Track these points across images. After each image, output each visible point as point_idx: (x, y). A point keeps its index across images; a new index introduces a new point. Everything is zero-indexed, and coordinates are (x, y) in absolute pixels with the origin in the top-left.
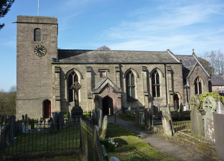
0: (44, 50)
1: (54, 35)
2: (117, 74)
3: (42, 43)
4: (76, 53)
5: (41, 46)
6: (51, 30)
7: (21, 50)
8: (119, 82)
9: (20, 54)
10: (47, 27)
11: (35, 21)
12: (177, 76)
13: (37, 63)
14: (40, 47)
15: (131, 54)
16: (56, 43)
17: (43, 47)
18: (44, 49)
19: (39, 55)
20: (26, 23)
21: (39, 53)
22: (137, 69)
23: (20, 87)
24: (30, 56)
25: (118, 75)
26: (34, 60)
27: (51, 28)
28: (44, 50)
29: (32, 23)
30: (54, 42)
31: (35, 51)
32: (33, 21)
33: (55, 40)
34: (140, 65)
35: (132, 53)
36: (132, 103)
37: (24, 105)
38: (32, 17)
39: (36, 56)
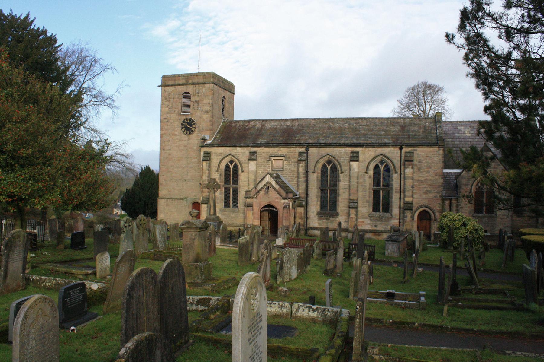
2: (300, 165)
7: (166, 127)
8: (303, 179)
9: (164, 132)
12: (428, 172)
13: (185, 146)
19: (187, 133)
20: (172, 85)
22: (341, 157)
24: (176, 135)
25: (302, 166)
29: (179, 85)
32: (181, 82)
34: (347, 148)
36: (327, 219)
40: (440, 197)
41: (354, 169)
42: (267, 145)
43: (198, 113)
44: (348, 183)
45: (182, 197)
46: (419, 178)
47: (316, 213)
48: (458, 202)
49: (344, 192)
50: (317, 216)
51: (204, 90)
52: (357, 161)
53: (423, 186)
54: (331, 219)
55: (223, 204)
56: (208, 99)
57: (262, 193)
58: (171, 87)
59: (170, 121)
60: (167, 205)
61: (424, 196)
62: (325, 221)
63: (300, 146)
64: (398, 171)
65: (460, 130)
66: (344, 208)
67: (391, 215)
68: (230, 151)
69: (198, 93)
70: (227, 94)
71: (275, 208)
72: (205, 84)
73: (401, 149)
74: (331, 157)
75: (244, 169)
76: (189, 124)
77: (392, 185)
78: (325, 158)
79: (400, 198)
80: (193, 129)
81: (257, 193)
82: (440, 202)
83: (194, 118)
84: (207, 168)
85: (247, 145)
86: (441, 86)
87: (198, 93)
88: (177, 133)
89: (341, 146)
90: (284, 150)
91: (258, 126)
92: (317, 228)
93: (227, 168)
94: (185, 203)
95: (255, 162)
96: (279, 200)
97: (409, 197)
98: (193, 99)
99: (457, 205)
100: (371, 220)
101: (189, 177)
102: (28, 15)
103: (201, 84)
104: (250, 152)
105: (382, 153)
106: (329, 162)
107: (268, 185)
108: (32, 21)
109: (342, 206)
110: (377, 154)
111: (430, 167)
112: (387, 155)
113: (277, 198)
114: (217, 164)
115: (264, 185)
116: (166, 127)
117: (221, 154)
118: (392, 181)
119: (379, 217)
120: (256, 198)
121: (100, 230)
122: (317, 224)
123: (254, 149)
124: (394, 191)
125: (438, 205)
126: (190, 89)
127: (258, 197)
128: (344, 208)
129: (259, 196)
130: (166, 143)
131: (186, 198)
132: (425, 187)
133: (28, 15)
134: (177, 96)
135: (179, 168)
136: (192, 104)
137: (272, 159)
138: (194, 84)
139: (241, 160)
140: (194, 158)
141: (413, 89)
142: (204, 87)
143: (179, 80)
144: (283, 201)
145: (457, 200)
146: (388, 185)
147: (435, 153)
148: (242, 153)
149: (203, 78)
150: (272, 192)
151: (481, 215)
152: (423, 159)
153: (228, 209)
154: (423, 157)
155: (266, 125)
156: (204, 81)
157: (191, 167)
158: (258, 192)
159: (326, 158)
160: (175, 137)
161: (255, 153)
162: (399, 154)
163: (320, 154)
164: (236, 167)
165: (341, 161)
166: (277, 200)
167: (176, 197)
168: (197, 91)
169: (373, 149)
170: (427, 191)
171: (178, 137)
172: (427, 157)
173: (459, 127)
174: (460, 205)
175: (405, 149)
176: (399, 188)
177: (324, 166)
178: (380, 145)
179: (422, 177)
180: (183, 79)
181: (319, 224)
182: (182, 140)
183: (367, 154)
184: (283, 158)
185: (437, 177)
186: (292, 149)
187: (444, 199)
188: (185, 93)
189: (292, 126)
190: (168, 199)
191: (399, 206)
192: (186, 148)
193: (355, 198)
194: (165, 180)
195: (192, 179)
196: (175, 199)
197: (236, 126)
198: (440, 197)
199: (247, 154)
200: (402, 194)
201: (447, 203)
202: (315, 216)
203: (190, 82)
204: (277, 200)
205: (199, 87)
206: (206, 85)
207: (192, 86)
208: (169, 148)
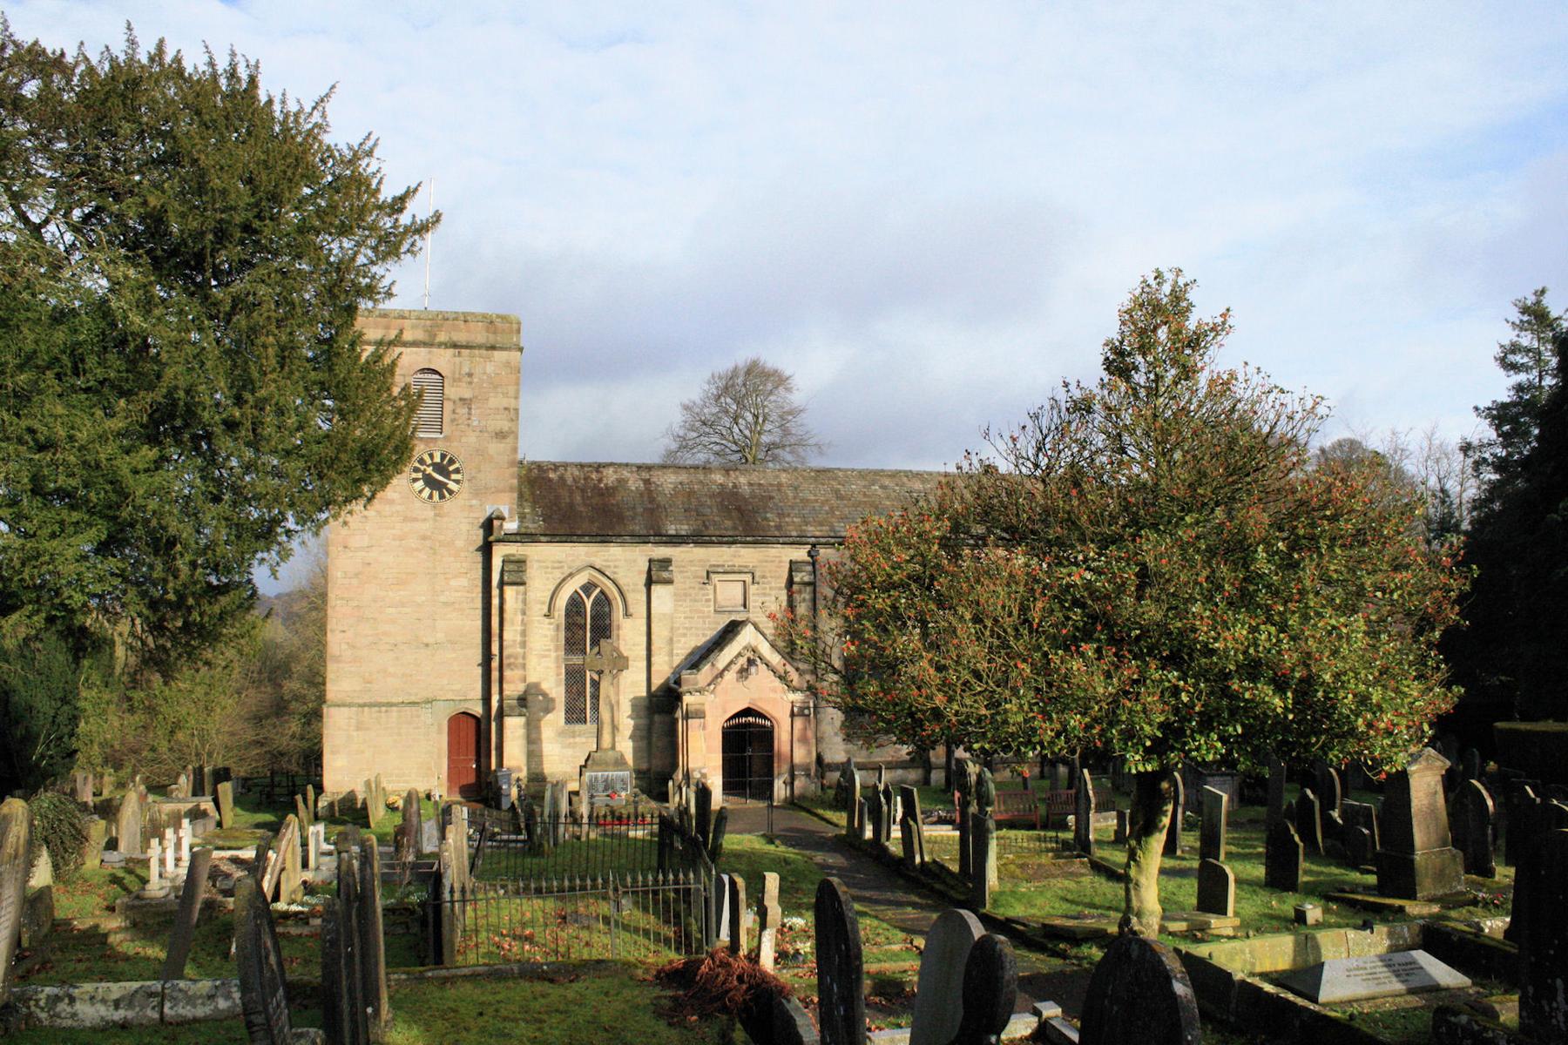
0: (454, 476)
1: (505, 402)
3: (446, 439)
4: (600, 480)
5: (443, 456)
6: (489, 376)
10: (466, 360)
11: (420, 335)
13: (424, 538)
14: (437, 459)
15: (880, 492)
16: (510, 440)
17: (452, 462)
18: (457, 471)
19: (431, 497)
21: (432, 488)
23: (344, 647)
26: (406, 519)
27: (490, 368)
28: (420, 475)
30: (501, 435)
31: (415, 480)
33: (505, 425)
35: (887, 482)
37: (358, 728)
38: (466, 318)
39: (418, 504)
42: (698, 538)
43: (472, 439)
45: (413, 699)
56: (506, 395)
57: (730, 676)
60: (359, 727)
63: (796, 543)
68: (587, 554)
72: (493, 348)
75: (631, 610)
76: (439, 468)
80: (452, 485)
83: (453, 450)
84: (520, 605)
85: (642, 539)
87: (470, 375)
90: (746, 555)
91: (634, 483)
93: (575, 605)
94: (425, 715)
95: (669, 588)
96: (778, 696)
101: (440, 636)
102: (161, 45)
103: (479, 347)
107: (750, 654)
108: (253, 81)
113: (774, 690)
115: (740, 654)
121: (1512, 871)
123: (662, 552)
131: (429, 701)
133: (161, 45)
135: (403, 605)
136: (448, 406)
139: (621, 582)
140: (455, 577)
148: (625, 562)
150: (761, 675)
153: (578, 727)
155: (654, 479)
156: (492, 339)
157: (445, 604)
158: (721, 674)
161: (666, 563)
164: (604, 601)
167: (394, 700)
168: (466, 370)
188: (423, 371)
189: (735, 486)
190: (363, 705)
192: (428, 543)
195: (452, 643)
196: (391, 705)
197: (562, 478)
203: (442, 337)
206: (496, 353)
207: (451, 351)
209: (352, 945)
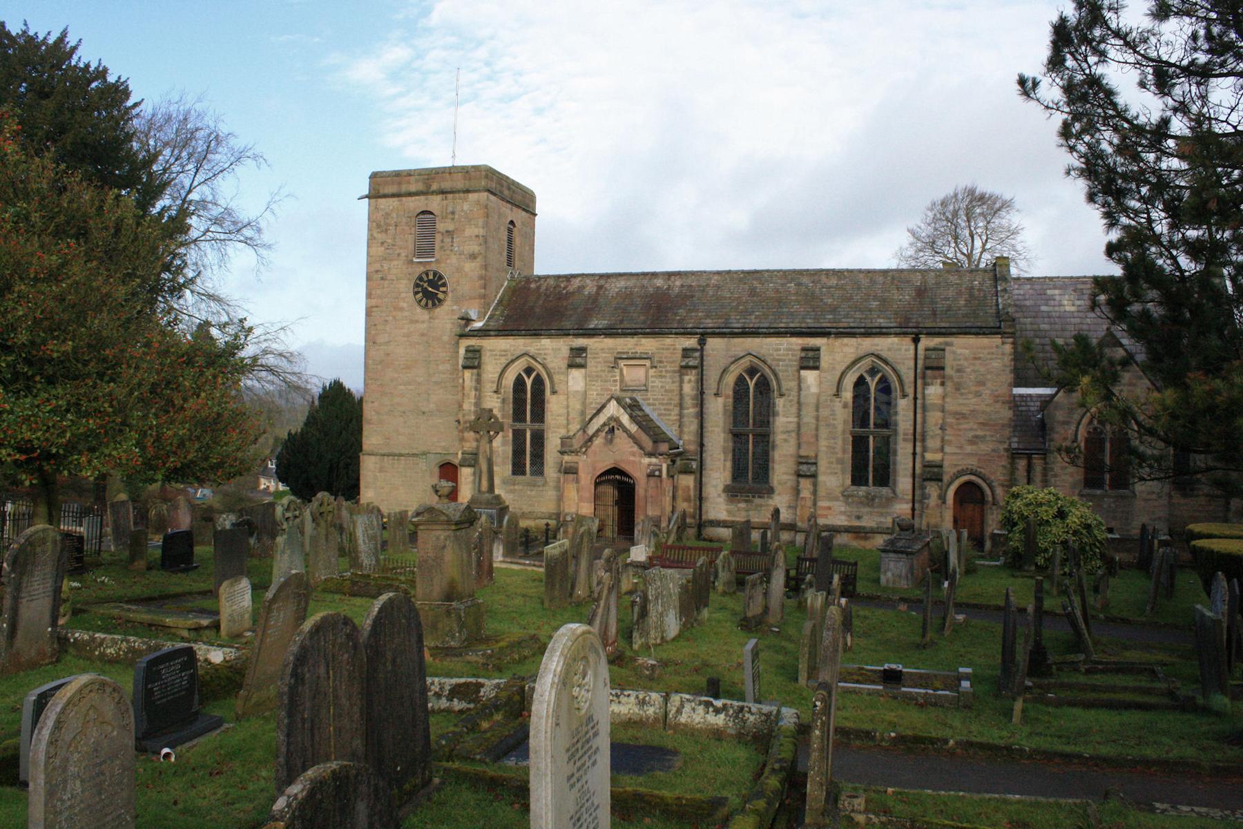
2: (686, 378)
7: (379, 292)
8: (692, 410)
9: (374, 302)
12: (978, 394)
13: (423, 335)
19: (427, 305)
20: (393, 196)
22: (779, 360)
24: (402, 309)
25: (690, 381)
29: (410, 194)
32: (413, 188)
34: (794, 340)
36: (746, 501)
40: (1006, 450)
41: (808, 387)
42: (610, 332)
43: (453, 260)
44: (796, 420)
45: (415, 451)
46: (958, 409)
47: (721, 487)
48: (1046, 463)
49: (786, 440)
50: (723, 495)
51: (466, 207)
52: (816, 368)
53: (966, 426)
54: (757, 501)
55: (509, 467)
56: (476, 226)
57: (598, 441)
58: (391, 200)
59: (389, 277)
60: (381, 470)
61: (969, 449)
62: (742, 505)
63: (687, 333)
64: (910, 391)
65: (1052, 298)
66: (785, 477)
67: (894, 492)
68: (525, 345)
69: (453, 213)
70: (519, 216)
71: (629, 477)
72: (468, 191)
73: (916, 341)
74: (756, 361)
75: (556, 388)
76: (431, 283)
77: (896, 425)
78: (742, 361)
79: (914, 454)
80: (441, 296)
81: (586, 442)
82: (1004, 462)
83: (444, 270)
84: (474, 384)
85: (564, 333)
86: (1007, 197)
87: (453, 213)
88: (405, 305)
89: (778, 334)
90: (648, 344)
91: (591, 288)
92: (725, 522)
93: (519, 384)
94: (422, 464)
95: (583, 370)
96: (637, 459)
97: (935, 451)
98: (441, 226)
99: (1045, 469)
100: (847, 503)
101: (432, 406)
102: (64, 34)
103: (459, 192)
104: (572, 349)
105: (873, 349)
106: (752, 371)
107: (613, 424)
108: (74, 49)
109: (781, 471)
110: (861, 353)
111: (982, 383)
112: (884, 354)
113: (633, 454)
114: (497, 375)
115: (604, 425)
116: (379, 292)
117: (504, 353)
118: (896, 413)
119: (867, 497)
120: (584, 453)
122: (725, 513)
123: (580, 342)
124: (900, 437)
125: (1000, 469)
126: (435, 203)
127: (590, 450)
128: (785, 477)
129: (593, 448)
130: (379, 327)
131: (424, 454)
132: (971, 429)
133: (64, 34)
134: (404, 220)
135: (409, 384)
136: (438, 237)
137: (622, 363)
138: (443, 192)
139: (550, 366)
140: (443, 363)
141: (944, 203)
142: (465, 199)
143: (409, 183)
144: (646, 460)
145: (1045, 459)
146: (886, 423)
147: (994, 350)
148: (552, 350)
149: (465, 178)
150: (621, 439)
151: (1099, 492)
152: (966, 364)
153: (520, 478)
154: (966, 359)
155: (607, 286)
156: (467, 185)
157: (436, 383)
158: (590, 439)
159: (745, 363)
160: (399, 315)
161: (582, 350)
162: (912, 352)
163: (731, 353)
164: (538, 382)
165: (780, 368)
166: (632, 458)
167: (403, 452)
168: (450, 209)
169: (852, 341)
170: (976, 437)
171: (406, 314)
172: (976, 359)
173: (1049, 292)
174: (1052, 469)
175: (925, 342)
176: (911, 431)
177: (740, 381)
178: (869, 333)
179: (964, 405)
180: (417, 181)
181: (729, 512)
182: (417, 322)
183: (839, 353)
184: (648, 363)
185: (998, 406)
186: (668, 341)
187: (1014, 455)
188: (423, 212)
190: (384, 455)
191: (911, 471)
192: (425, 338)
193: (812, 454)
194: (378, 413)
195: (439, 411)
196: (401, 455)
197: (538, 288)
198: (1006, 450)
199: (565, 352)
200: (918, 444)
201: (1022, 464)
202: (719, 496)
203: (435, 187)
204: (632, 458)
205: (454, 199)
206: (470, 195)
207: (439, 197)
208: (387, 340)
209: (1088, 672)
